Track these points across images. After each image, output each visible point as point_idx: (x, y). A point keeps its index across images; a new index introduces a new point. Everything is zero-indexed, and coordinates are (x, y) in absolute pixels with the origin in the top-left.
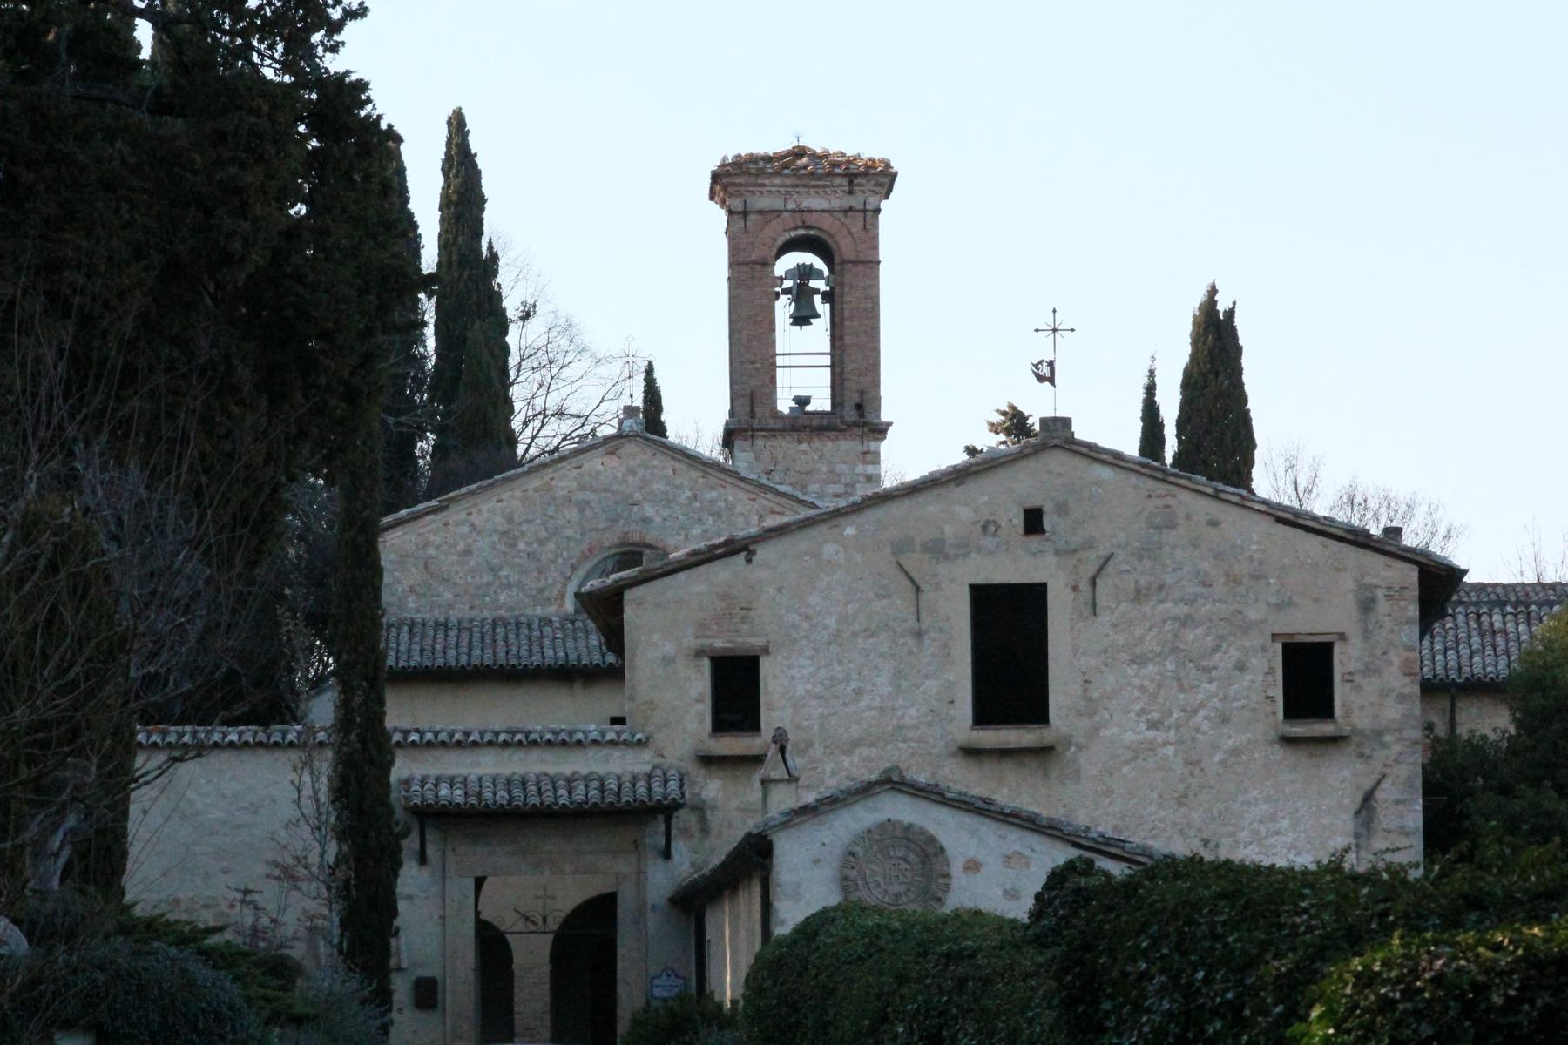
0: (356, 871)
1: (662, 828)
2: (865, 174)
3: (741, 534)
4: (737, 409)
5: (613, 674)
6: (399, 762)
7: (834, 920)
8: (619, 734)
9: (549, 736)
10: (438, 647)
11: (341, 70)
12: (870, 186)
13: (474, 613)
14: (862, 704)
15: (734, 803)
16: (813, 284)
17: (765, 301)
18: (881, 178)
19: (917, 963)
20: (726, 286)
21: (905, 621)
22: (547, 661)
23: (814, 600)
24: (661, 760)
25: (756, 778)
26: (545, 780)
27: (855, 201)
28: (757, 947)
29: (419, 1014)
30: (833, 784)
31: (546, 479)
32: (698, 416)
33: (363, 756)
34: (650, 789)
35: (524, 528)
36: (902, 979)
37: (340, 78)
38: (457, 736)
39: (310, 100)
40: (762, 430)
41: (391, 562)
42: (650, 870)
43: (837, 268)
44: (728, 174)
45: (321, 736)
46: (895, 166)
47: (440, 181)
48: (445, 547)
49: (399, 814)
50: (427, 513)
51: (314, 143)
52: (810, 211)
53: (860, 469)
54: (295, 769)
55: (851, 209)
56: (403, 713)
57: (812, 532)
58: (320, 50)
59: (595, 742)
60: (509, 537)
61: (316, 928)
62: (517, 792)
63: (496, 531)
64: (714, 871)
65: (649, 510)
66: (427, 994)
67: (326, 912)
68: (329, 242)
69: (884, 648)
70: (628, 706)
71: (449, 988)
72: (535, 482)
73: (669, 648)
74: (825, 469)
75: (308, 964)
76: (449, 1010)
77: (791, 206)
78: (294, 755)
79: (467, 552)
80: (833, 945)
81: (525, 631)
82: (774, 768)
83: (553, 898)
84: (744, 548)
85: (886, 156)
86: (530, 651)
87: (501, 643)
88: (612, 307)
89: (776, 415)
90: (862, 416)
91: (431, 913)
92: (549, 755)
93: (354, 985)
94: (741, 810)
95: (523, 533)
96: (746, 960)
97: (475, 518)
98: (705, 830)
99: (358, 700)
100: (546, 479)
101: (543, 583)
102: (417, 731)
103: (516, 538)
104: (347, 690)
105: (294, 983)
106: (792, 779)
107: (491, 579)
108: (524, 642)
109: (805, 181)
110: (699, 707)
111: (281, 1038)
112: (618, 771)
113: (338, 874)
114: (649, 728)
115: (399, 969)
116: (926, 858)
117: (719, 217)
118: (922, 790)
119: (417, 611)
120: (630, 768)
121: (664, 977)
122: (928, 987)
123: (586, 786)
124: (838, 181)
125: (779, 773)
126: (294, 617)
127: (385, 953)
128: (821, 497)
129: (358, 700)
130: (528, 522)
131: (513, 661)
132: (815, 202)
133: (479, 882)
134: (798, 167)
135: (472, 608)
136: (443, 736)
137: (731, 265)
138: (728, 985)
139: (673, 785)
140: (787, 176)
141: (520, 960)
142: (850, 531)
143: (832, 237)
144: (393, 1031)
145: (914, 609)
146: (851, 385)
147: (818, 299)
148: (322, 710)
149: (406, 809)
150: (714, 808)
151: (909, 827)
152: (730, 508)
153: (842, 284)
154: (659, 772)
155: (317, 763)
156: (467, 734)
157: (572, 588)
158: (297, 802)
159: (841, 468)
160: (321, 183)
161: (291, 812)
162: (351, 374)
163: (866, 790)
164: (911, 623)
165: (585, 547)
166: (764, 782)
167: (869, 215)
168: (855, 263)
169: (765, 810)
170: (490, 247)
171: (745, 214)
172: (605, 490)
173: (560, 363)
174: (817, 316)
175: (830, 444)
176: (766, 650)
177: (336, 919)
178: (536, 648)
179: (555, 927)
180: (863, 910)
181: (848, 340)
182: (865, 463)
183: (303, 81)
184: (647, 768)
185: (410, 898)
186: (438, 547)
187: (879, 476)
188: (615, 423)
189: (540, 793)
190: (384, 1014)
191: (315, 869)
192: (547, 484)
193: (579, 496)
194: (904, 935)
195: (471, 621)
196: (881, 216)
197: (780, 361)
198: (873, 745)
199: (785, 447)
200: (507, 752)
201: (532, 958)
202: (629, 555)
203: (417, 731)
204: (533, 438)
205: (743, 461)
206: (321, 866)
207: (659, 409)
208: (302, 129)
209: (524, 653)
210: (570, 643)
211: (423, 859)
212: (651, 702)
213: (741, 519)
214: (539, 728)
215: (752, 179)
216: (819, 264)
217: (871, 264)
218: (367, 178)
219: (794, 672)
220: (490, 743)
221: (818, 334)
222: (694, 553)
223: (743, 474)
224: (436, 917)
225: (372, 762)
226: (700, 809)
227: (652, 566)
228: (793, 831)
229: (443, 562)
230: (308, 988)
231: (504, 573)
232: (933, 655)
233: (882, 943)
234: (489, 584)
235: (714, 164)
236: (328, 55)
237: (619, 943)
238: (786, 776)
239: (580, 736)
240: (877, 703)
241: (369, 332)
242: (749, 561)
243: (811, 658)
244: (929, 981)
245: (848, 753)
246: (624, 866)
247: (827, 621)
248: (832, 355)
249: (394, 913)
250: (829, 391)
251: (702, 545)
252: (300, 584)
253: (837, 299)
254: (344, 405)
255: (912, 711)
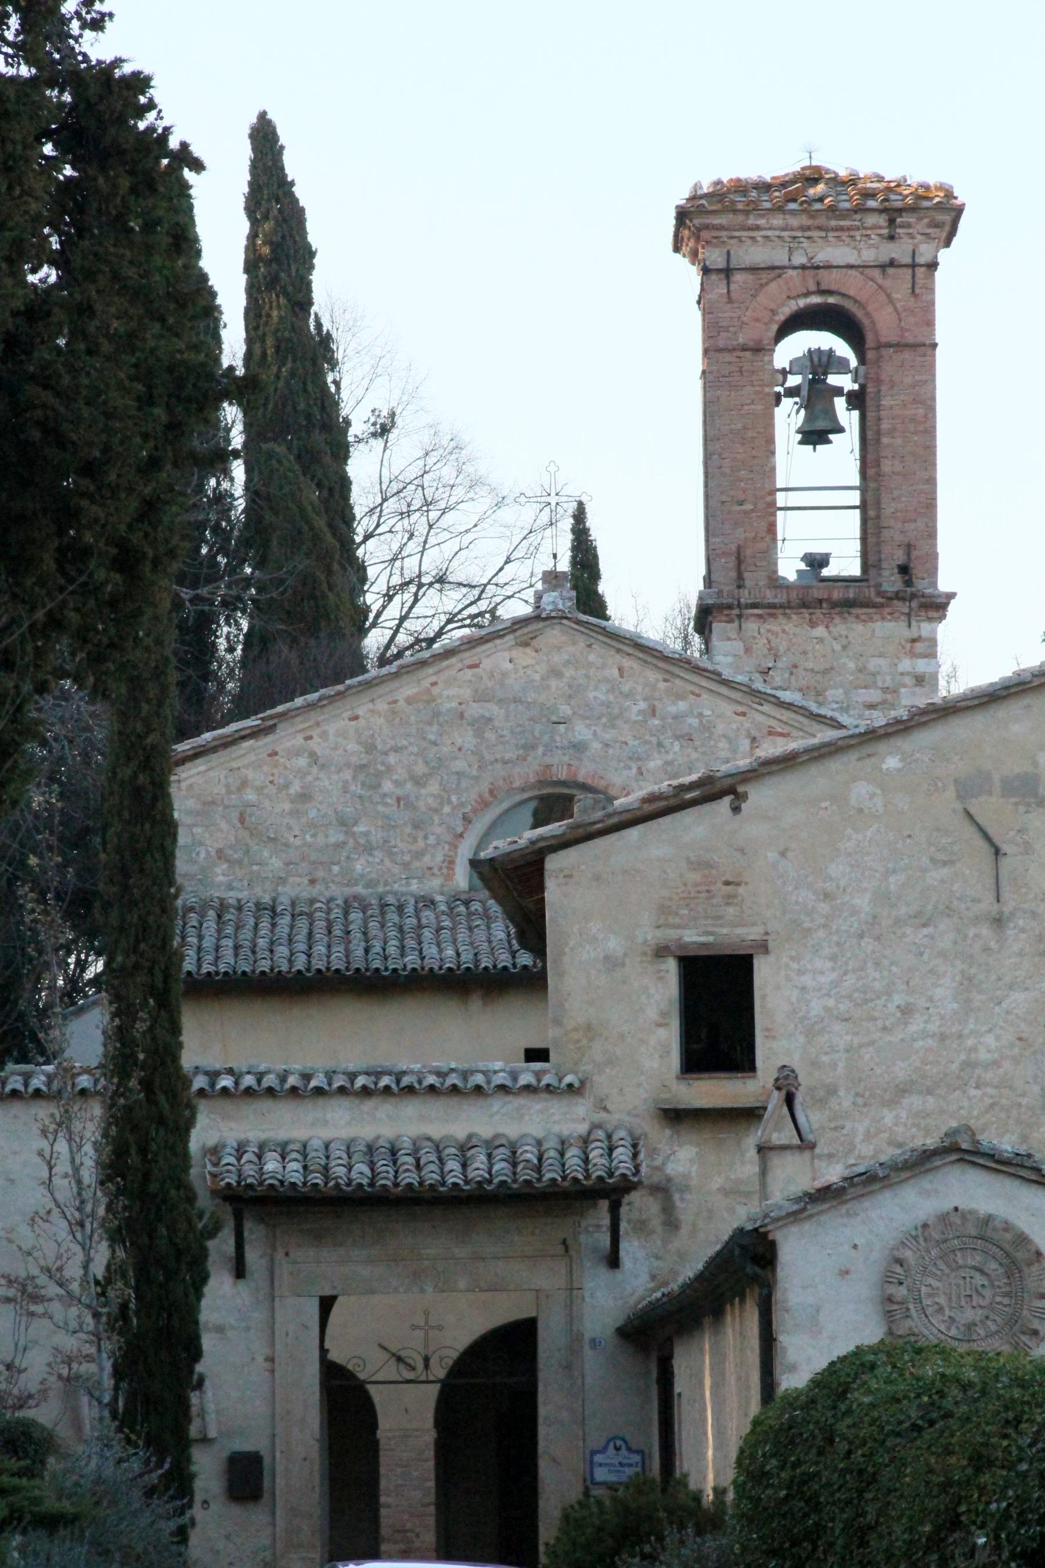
0: (137, 1289)
1: (606, 1221)
2: (913, 209)
3: (724, 768)
4: (714, 577)
5: (532, 982)
6: (202, 1120)
7: (873, 1367)
8: (538, 1075)
9: (431, 1079)
10: (262, 943)
11: (108, 58)
12: (921, 226)
13: (315, 891)
14: (913, 1028)
15: (717, 1182)
16: (833, 380)
17: (759, 407)
18: (937, 214)
19: (1005, 1436)
20: (698, 384)
21: (977, 900)
22: (428, 963)
23: (837, 869)
24: (603, 1115)
25: (751, 1141)
26: (427, 1147)
27: (899, 251)
28: (755, 1408)
29: (236, 1510)
30: (868, 1151)
31: (426, 683)
32: (655, 584)
33: (149, 1106)
34: (586, 1160)
35: (392, 759)
36: (980, 1462)
37: (105, 72)
38: (292, 1081)
39: (62, 105)
40: (754, 606)
41: (189, 812)
42: (589, 1285)
43: (870, 355)
44: (701, 211)
45: (84, 1081)
46: (962, 195)
47: (244, 226)
48: (272, 789)
49: (204, 1201)
50: (243, 738)
51: (68, 171)
52: (829, 267)
53: (905, 664)
54: (44, 1133)
55: (892, 263)
56: (208, 1043)
57: (834, 765)
58: (75, 26)
59: (502, 1088)
60: (369, 773)
61: (78, 1377)
62: (383, 1166)
63: (348, 765)
64: (685, 1287)
65: (582, 731)
66: (246, 1478)
67: (93, 1350)
68: (92, 327)
69: (945, 942)
70: (553, 1033)
71: (280, 1468)
72: (406, 689)
73: (614, 944)
74: (851, 665)
75: (64, 1433)
76: (280, 1503)
77: (799, 259)
78: (44, 1111)
79: (305, 797)
80: (873, 1406)
81: (393, 917)
82: (778, 1128)
83: (440, 1328)
84: (731, 791)
85: (947, 180)
86: (402, 948)
87: (357, 936)
88: (511, 407)
89: (776, 582)
90: (909, 583)
91: (252, 1355)
92: (435, 1107)
93: (136, 1465)
94: (726, 1192)
95: (389, 769)
96: (738, 1428)
97: (316, 745)
98: (672, 1224)
99: (141, 1026)
100: (426, 683)
101: (421, 843)
102: (230, 1071)
103: (379, 775)
104: (124, 1012)
105: (43, 1463)
106: (805, 1145)
107: (341, 838)
108: (393, 933)
109: (822, 221)
110: (662, 1032)
111: (22, 1550)
112: (539, 1134)
113: (111, 1293)
114: (586, 1068)
115: (205, 1440)
116: (1013, 1268)
117: (687, 277)
118: (1007, 1163)
119: (230, 887)
120: (556, 1129)
121: (611, 1450)
122: (1024, 1475)
123: (489, 1156)
124: (871, 220)
125: (786, 1135)
126: (42, 899)
127: (182, 1412)
128: (845, 710)
129: (141, 1026)
130: (396, 750)
131: (377, 964)
132: (836, 252)
133: (326, 1304)
134: (809, 198)
135: (312, 882)
136: (270, 1080)
137: (706, 352)
138: (710, 1463)
139: (622, 1154)
140: (792, 212)
141: (386, 1425)
142: (892, 763)
143: (862, 306)
144: (195, 1538)
145: (990, 882)
146: (893, 535)
147: (840, 403)
148: (85, 1039)
149: (214, 1193)
150: (686, 1188)
151: (988, 1219)
152: (707, 727)
153: (879, 381)
154: (600, 1134)
155: (77, 1126)
156: (307, 1077)
157: (465, 851)
158: (49, 1185)
159: (873, 664)
160: (81, 233)
161: (37, 1198)
162: (130, 526)
163: (920, 1162)
164: (987, 904)
165: (484, 787)
166: (762, 1150)
167: (920, 272)
168: (900, 346)
169: (764, 1195)
170: (319, 325)
171: (727, 272)
172: (516, 700)
173: (442, 505)
174: (841, 430)
175: (859, 628)
176: (764, 947)
177: (108, 1365)
178: (410, 943)
179: (441, 1374)
180: (919, 1351)
181: (887, 467)
182: (913, 655)
183: (51, 75)
184: (583, 1128)
185: (220, 1329)
186: (259, 790)
187: (934, 677)
188: (529, 595)
189: (418, 1167)
190: (181, 1512)
191: (75, 1287)
192: (428, 691)
193: (475, 710)
194: (984, 1392)
195: (312, 901)
196: (939, 274)
197: (781, 499)
198: (929, 1092)
199: (792, 632)
200: (369, 1104)
201: (407, 1423)
202: (552, 804)
203: (230, 1071)
204: (403, 619)
205: (727, 653)
206: (84, 1281)
207: (595, 575)
208: (48, 149)
209: (392, 950)
210: (462, 935)
211: (240, 1271)
212: (589, 1027)
213: (723, 744)
214: (417, 1067)
215: (740, 218)
216: (842, 349)
217: (924, 348)
218: (149, 226)
219: (807, 980)
220: (342, 1090)
221: (841, 458)
222: (652, 798)
223: (727, 674)
224: (260, 1359)
225: (161, 1121)
226: (663, 1190)
227: (587, 819)
228: (806, 1226)
229: (264, 813)
230: (67, 1471)
231: (360, 828)
232: (1021, 954)
233: (948, 1403)
234: (340, 846)
235: (680, 196)
236: (88, 34)
237: (541, 1399)
238: (796, 1141)
239: (479, 1079)
240: (933, 1027)
241: (154, 464)
242: (736, 809)
243: (833, 958)
244: (1024, 1467)
245: (891, 1103)
246: (547, 1278)
247: (857, 901)
248: (863, 489)
249: (195, 1353)
250: (857, 545)
251: (664, 786)
252: (50, 848)
253: (869, 403)
254: (117, 577)
255: (990, 1040)
